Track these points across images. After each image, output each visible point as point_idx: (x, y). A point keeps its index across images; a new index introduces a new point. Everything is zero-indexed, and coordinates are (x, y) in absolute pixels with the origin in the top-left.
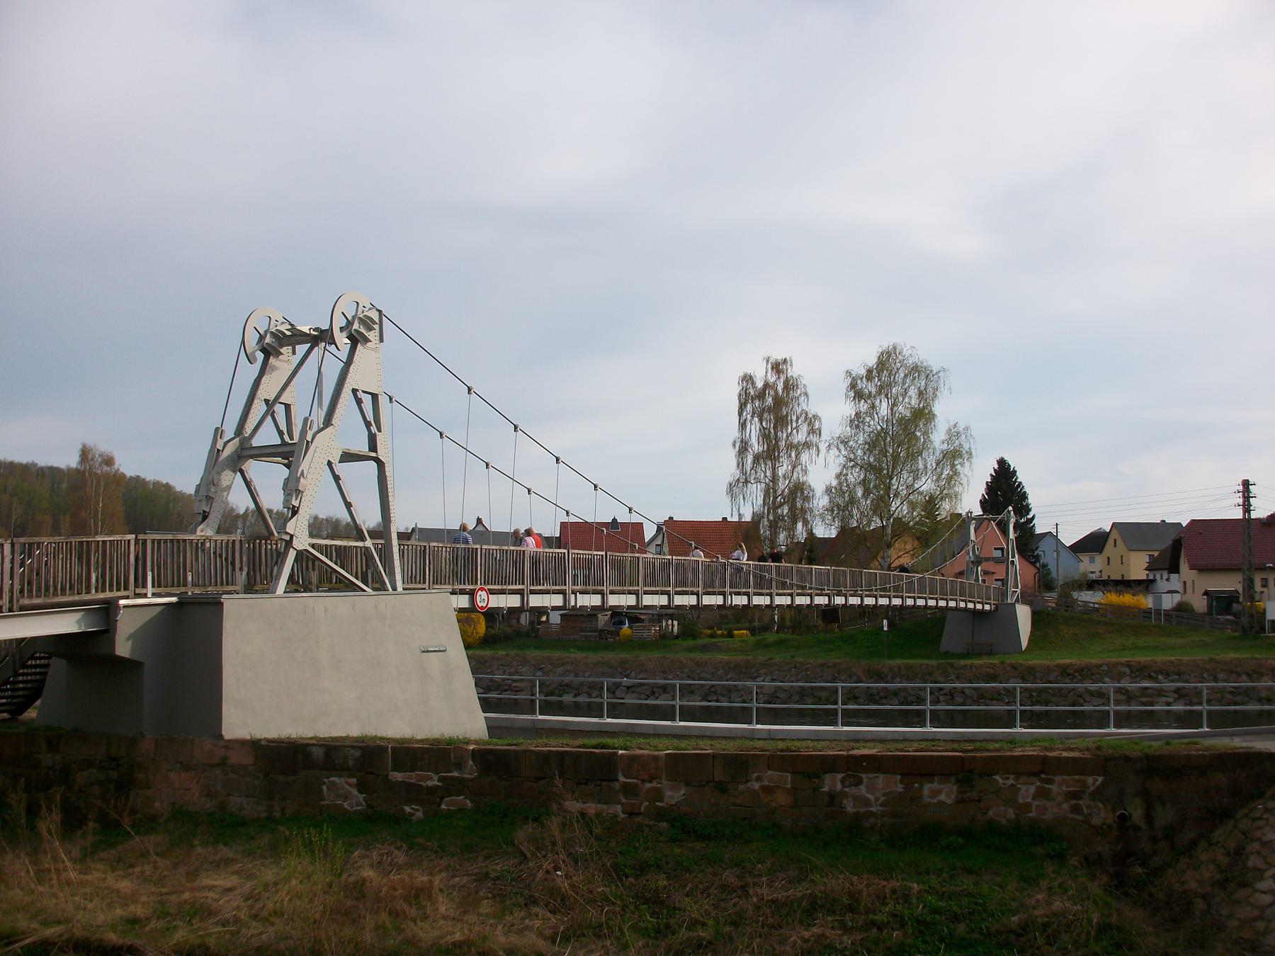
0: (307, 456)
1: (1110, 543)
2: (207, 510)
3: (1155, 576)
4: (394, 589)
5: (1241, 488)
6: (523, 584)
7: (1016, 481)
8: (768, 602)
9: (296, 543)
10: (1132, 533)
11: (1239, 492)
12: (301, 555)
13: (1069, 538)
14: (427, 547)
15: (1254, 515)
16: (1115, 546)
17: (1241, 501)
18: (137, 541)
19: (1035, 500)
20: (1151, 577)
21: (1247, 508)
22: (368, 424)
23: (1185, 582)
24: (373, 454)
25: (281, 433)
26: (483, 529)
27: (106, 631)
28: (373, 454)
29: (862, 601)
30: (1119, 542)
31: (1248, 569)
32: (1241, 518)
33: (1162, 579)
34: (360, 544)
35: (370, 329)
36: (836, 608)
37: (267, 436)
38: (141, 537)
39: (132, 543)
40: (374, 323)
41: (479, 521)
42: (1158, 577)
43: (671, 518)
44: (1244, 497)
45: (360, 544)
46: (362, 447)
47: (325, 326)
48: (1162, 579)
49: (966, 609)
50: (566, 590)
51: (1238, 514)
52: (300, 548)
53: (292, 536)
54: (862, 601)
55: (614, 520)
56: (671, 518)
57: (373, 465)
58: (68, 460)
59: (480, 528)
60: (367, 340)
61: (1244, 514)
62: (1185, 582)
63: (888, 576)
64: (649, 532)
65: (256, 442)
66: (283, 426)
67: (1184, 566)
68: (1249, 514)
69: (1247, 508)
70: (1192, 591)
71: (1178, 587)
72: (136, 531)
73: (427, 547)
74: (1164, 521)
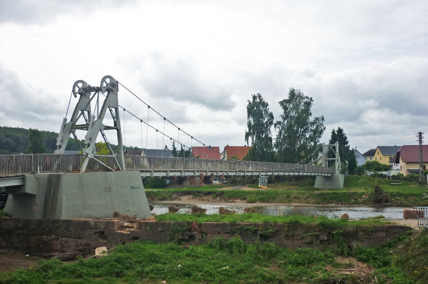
0: (93, 128)
1: (376, 153)
2: (61, 145)
3: (392, 164)
4: (123, 170)
5: (418, 135)
6: (151, 168)
7: (343, 133)
8: (272, 174)
9: (89, 156)
10: (384, 150)
11: (418, 136)
12: (91, 160)
13: (363, 151)
14: (135, 157)
15: (423, 144)
16: (378, 154)
17: (418, 139)
18: (34, 156)
19: (349, 139)
20: (391, 165)
21: (421, 142)
22: (114, 118)
23: (401, 166)
24: (116, 127)
25: (86, 120)
26: (167, 149)
27: (24, 185)
28: (116, 127)
29: (315, 174)
30: (380, 153)
31: (421, 162)
32: (419, 145)
33: (394, 165)
34: (111, 156)
35: (114, 87)
36: (286, 176)
37: (81, 121)
38: (35, 154)
39: (33, 156)
40: (115, 85)
41: (166, 146)
42: (393, 164)
43: (228, 145)
44: (419, 138)
45: (111, 156)
46: (112, 125)
47: (99, 87)
48: (394, 165)
49: (321, 176)
50: (151, 170)
51: (418, 144)
52: (91, 157)
53: (87, 154)
54: (315, 174)
55: (210, 146)
56: (228, 145)
57: (115, 131)
58: (17, 127)
59: (166, 149)
60: (113, 91)
61: (420, 144)
62: (401, 166)
63: (288, 165)
64: (222, 150)
65: (77, 124)
66: (87, 118)
67: (401, 161)
68: (421, 144)
69: (421, 142)
70: (403, 169)
71: (399, 168)
72: (34, 153)
73: (135, 157)
74: (395, 146)
